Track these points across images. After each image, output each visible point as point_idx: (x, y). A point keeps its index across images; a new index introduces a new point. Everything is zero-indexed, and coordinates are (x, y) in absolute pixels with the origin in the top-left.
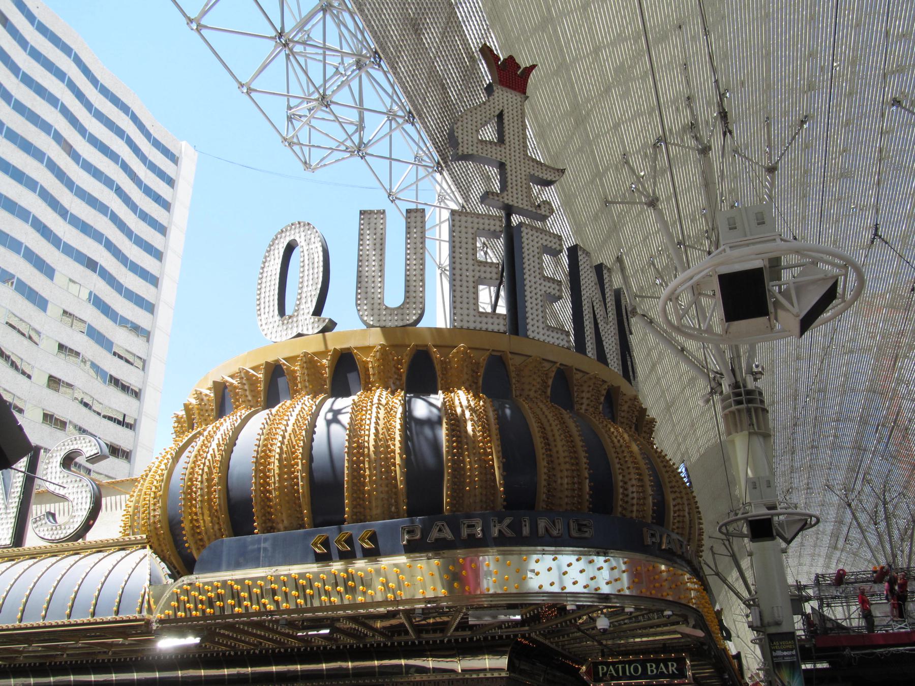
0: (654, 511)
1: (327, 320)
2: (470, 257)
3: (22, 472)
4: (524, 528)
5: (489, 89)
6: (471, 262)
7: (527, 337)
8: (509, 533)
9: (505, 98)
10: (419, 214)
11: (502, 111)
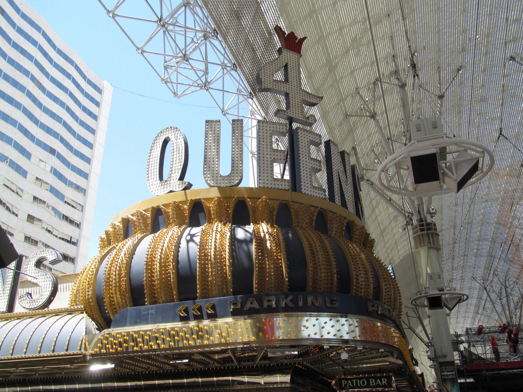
0: (374, 292)
1: (187, 183)
2: (269, 147)
3: (12, 270)
4: (299, 302)
5: (280, 51)
6: (269, 150)
7: (301, 192)
8: (291, 305)
9: (289, 56)
10: (239, 122)
11: (287, 63)
